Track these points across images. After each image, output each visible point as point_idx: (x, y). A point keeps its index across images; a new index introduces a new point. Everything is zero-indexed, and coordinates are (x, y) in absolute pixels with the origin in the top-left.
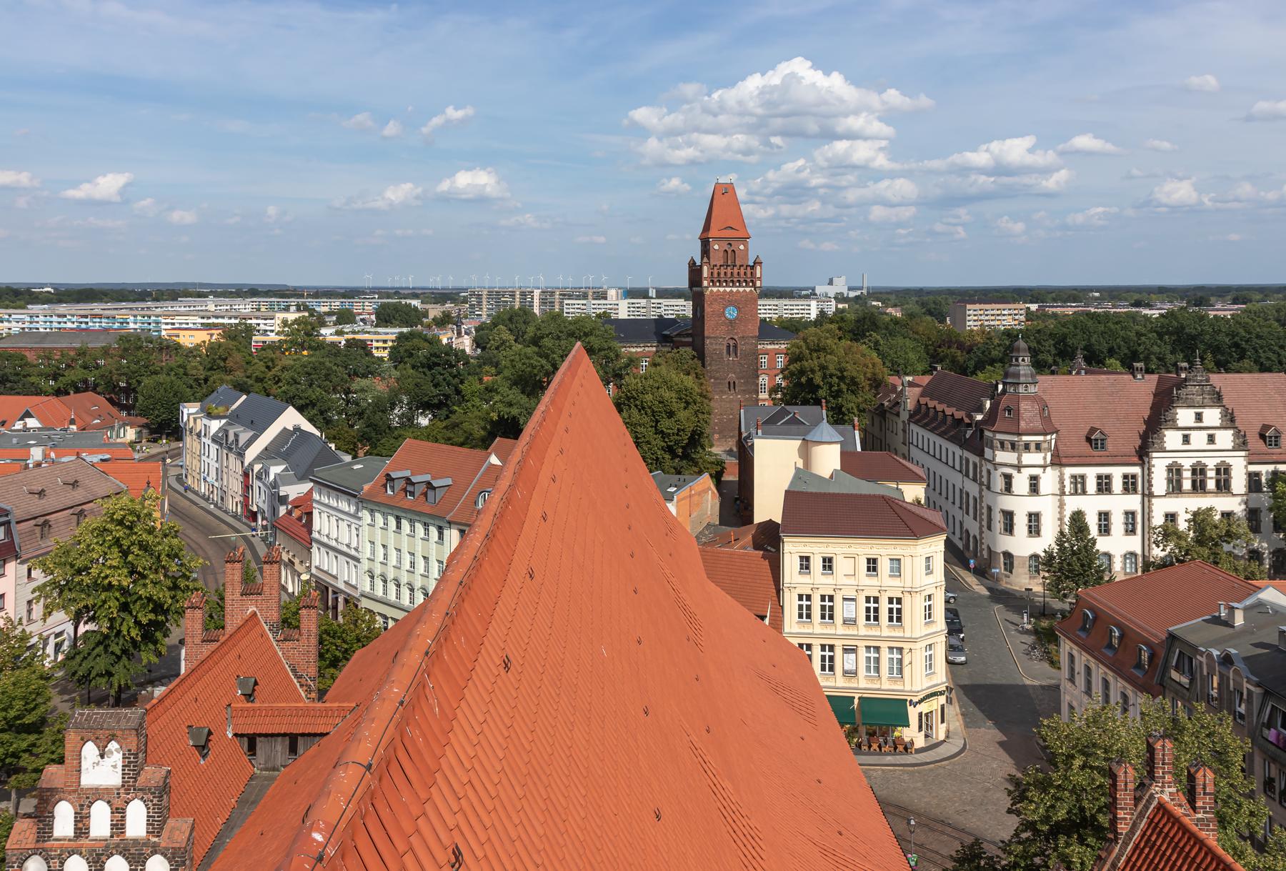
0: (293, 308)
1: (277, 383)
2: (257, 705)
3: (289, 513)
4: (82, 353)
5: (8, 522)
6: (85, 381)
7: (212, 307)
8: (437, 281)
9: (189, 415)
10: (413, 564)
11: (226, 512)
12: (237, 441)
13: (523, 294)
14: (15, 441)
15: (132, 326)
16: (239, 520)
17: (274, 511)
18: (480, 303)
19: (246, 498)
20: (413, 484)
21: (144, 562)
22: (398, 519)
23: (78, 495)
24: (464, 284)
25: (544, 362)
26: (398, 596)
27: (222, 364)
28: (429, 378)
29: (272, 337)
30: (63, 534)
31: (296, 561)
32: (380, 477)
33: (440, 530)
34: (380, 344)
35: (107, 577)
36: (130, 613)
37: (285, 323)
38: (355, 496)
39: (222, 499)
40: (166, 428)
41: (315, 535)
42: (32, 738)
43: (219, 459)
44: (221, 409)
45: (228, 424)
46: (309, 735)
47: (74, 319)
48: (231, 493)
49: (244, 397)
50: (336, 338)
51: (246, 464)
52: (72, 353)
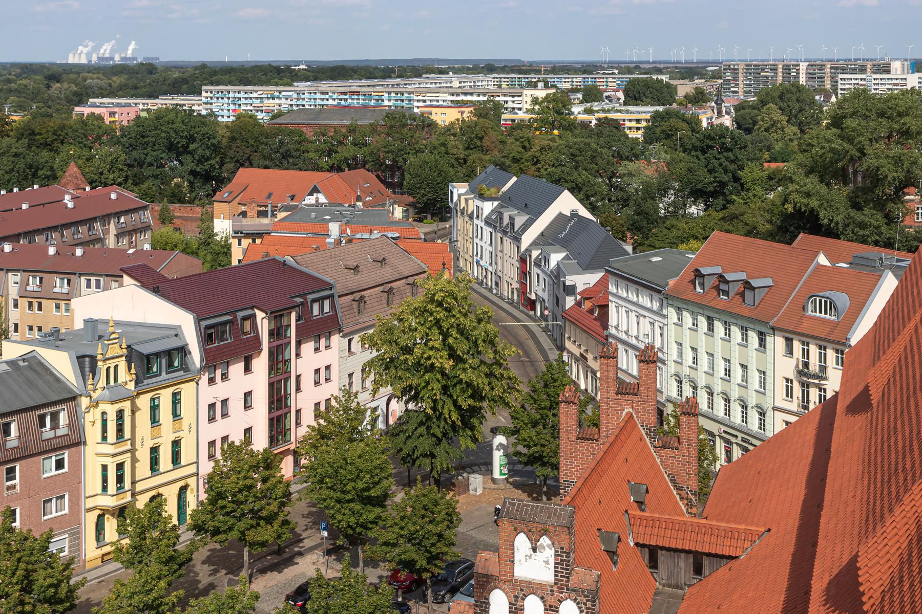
0: (540, 85)
1: (535, 164)
2: (646, 514)
3: (579, 304)
4: (352, 130)
5: (332, 296)
6: (355, 158)
7: (456, 84)
8: (682, 54)
9: (459, 196)
10: (728, 372)
11: (501, 298)
12: (512, 224)
13: (787, 68)
14: (313, 215)
15: (386, 103)
16: (516, 307)
17: (558, 301)
18: (736, 79)
19: (523, 285)
20: (728, 282)
21: (462, 347)
22: (710, 320)
23: (386, 273)
24: (711, 57)
25: (847, 146)
26: (727, 412)
27: (479, 143)
28: (703, 162)
29: (521, 115)
30: (379, 312)
31: (590, 357)
32: (686, 272)
33: (762, 336)
34: (633, 124)
35: (429, 358)
36: (451, 396)
37: (535, 101)
38: (659, 292)
39: (497, 284)
40: (433, 207)
41: (612, 331)
42: (378, 510)
43: (493, 244)
44: (493, 190)
45: (500, 206)
46: (716, 556)
47: (335, 96)
48: (506, 278)
49: (514, 179)
50: (585, 117)
51: (523, 249)
52: (344, 130)
